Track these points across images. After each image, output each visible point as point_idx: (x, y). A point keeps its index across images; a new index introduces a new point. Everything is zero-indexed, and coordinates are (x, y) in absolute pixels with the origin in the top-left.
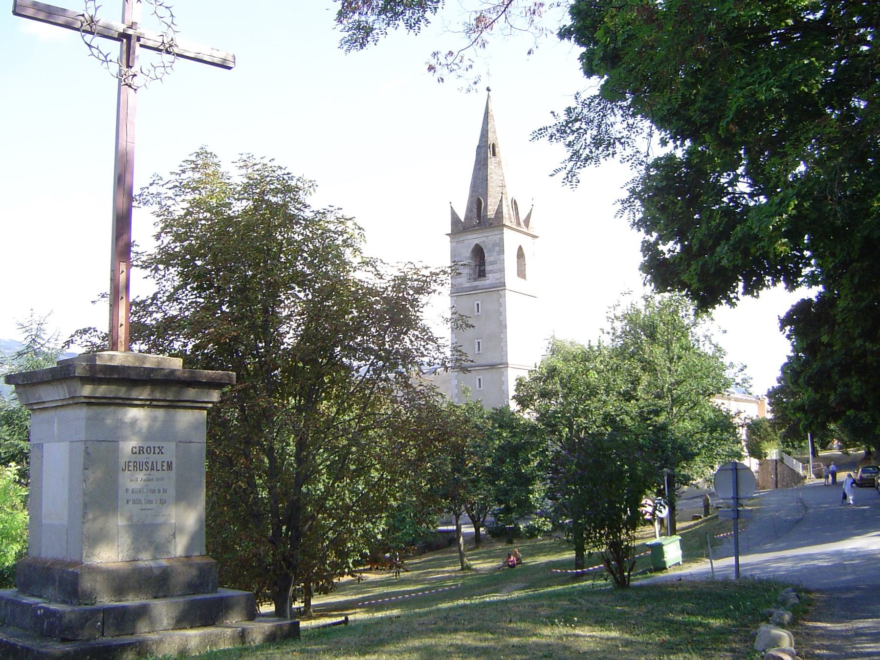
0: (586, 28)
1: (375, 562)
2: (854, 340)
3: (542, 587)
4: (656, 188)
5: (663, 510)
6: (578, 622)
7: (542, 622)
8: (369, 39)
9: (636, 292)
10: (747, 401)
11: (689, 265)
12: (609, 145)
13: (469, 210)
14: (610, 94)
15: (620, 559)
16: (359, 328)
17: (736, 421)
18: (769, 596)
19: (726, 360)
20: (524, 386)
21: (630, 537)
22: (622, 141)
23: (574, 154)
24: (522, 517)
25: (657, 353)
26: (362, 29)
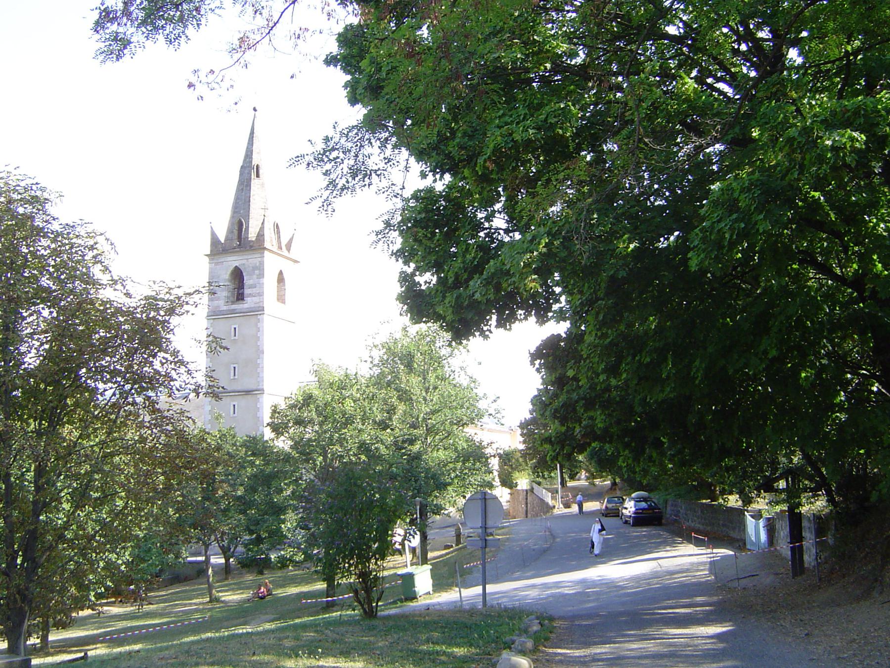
0: (353, 57)
1: (118, 594)
2: (598, 375)
3: (293, 619)
4: (416, 220)
5: (412, 539)
6: (322, 653)
7: (286, 654)
8: (125, 51)
9: (394, 323)
10: (500, 431)
11: (444, 297)
12: (365, 176)
13: (230, 231)
14: (372, 124)
15: (368, 589)
16: (106, 349)
17: (488, 451)
18: (513, 624)
19: (480, 392)
20: (279, 413)
21: (379, 567)
22: (378, 173)
23: (331, 183)
24: (273, 548)
25: (413, 383)
26: (120, 40)
